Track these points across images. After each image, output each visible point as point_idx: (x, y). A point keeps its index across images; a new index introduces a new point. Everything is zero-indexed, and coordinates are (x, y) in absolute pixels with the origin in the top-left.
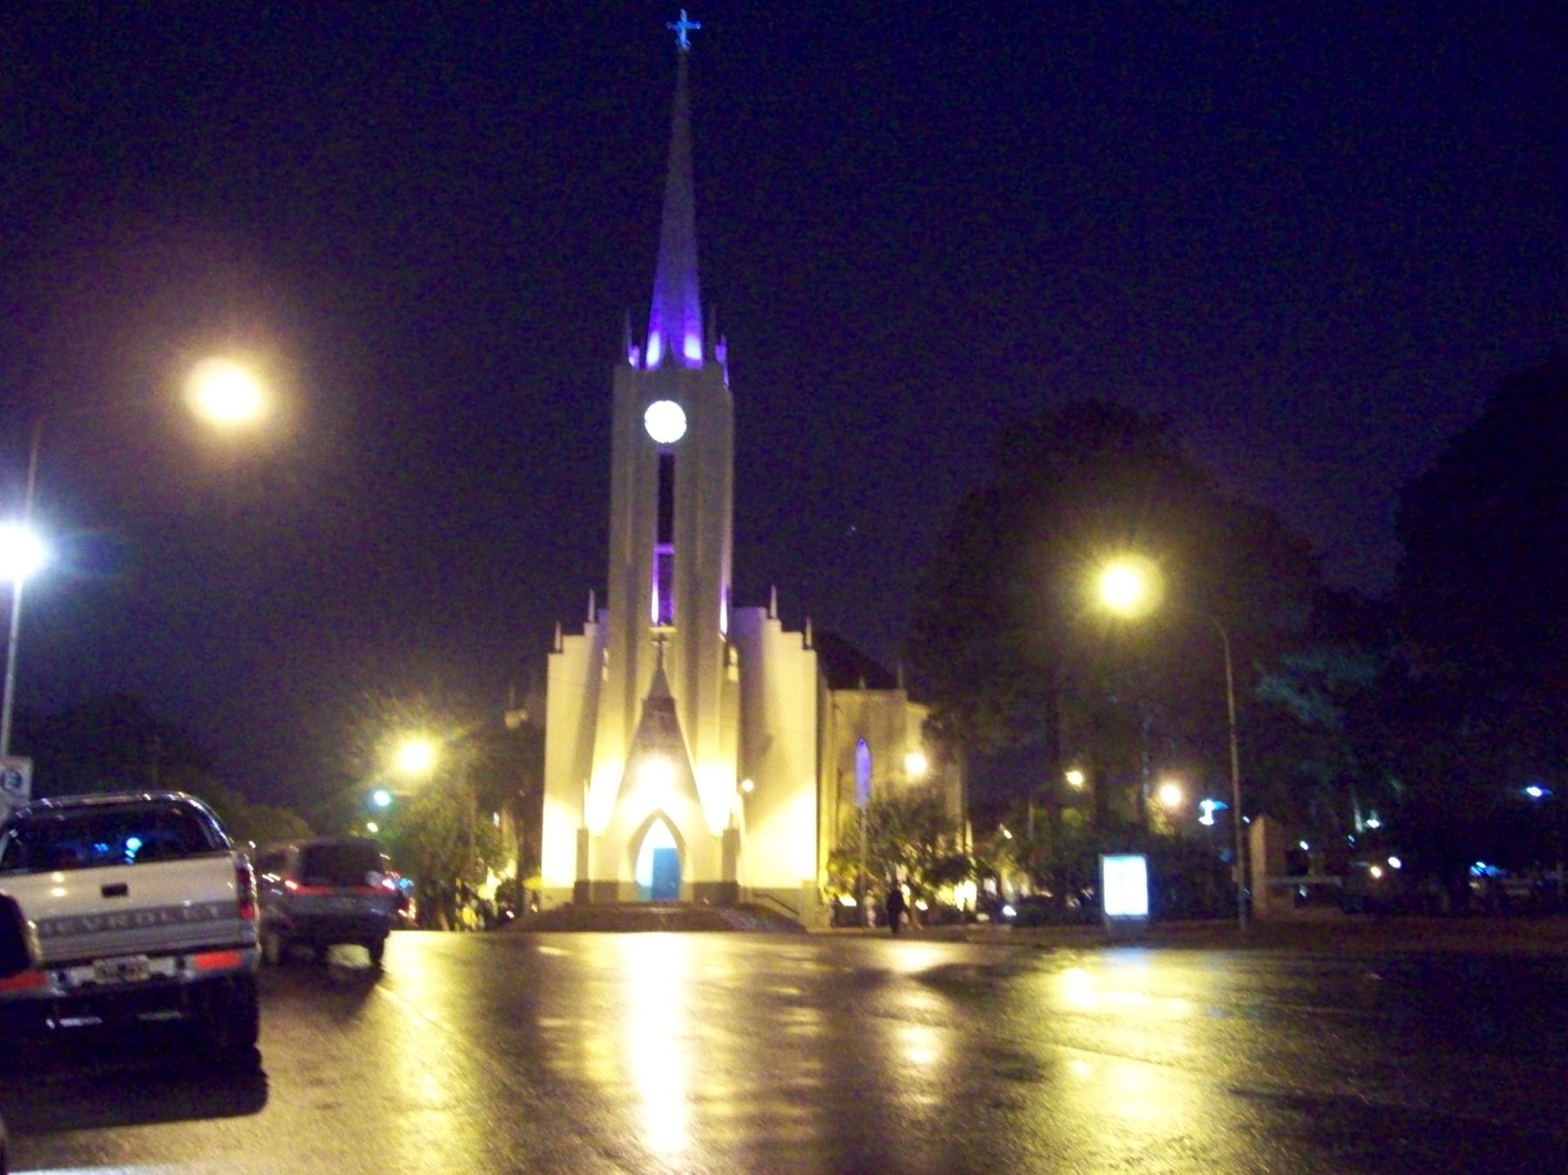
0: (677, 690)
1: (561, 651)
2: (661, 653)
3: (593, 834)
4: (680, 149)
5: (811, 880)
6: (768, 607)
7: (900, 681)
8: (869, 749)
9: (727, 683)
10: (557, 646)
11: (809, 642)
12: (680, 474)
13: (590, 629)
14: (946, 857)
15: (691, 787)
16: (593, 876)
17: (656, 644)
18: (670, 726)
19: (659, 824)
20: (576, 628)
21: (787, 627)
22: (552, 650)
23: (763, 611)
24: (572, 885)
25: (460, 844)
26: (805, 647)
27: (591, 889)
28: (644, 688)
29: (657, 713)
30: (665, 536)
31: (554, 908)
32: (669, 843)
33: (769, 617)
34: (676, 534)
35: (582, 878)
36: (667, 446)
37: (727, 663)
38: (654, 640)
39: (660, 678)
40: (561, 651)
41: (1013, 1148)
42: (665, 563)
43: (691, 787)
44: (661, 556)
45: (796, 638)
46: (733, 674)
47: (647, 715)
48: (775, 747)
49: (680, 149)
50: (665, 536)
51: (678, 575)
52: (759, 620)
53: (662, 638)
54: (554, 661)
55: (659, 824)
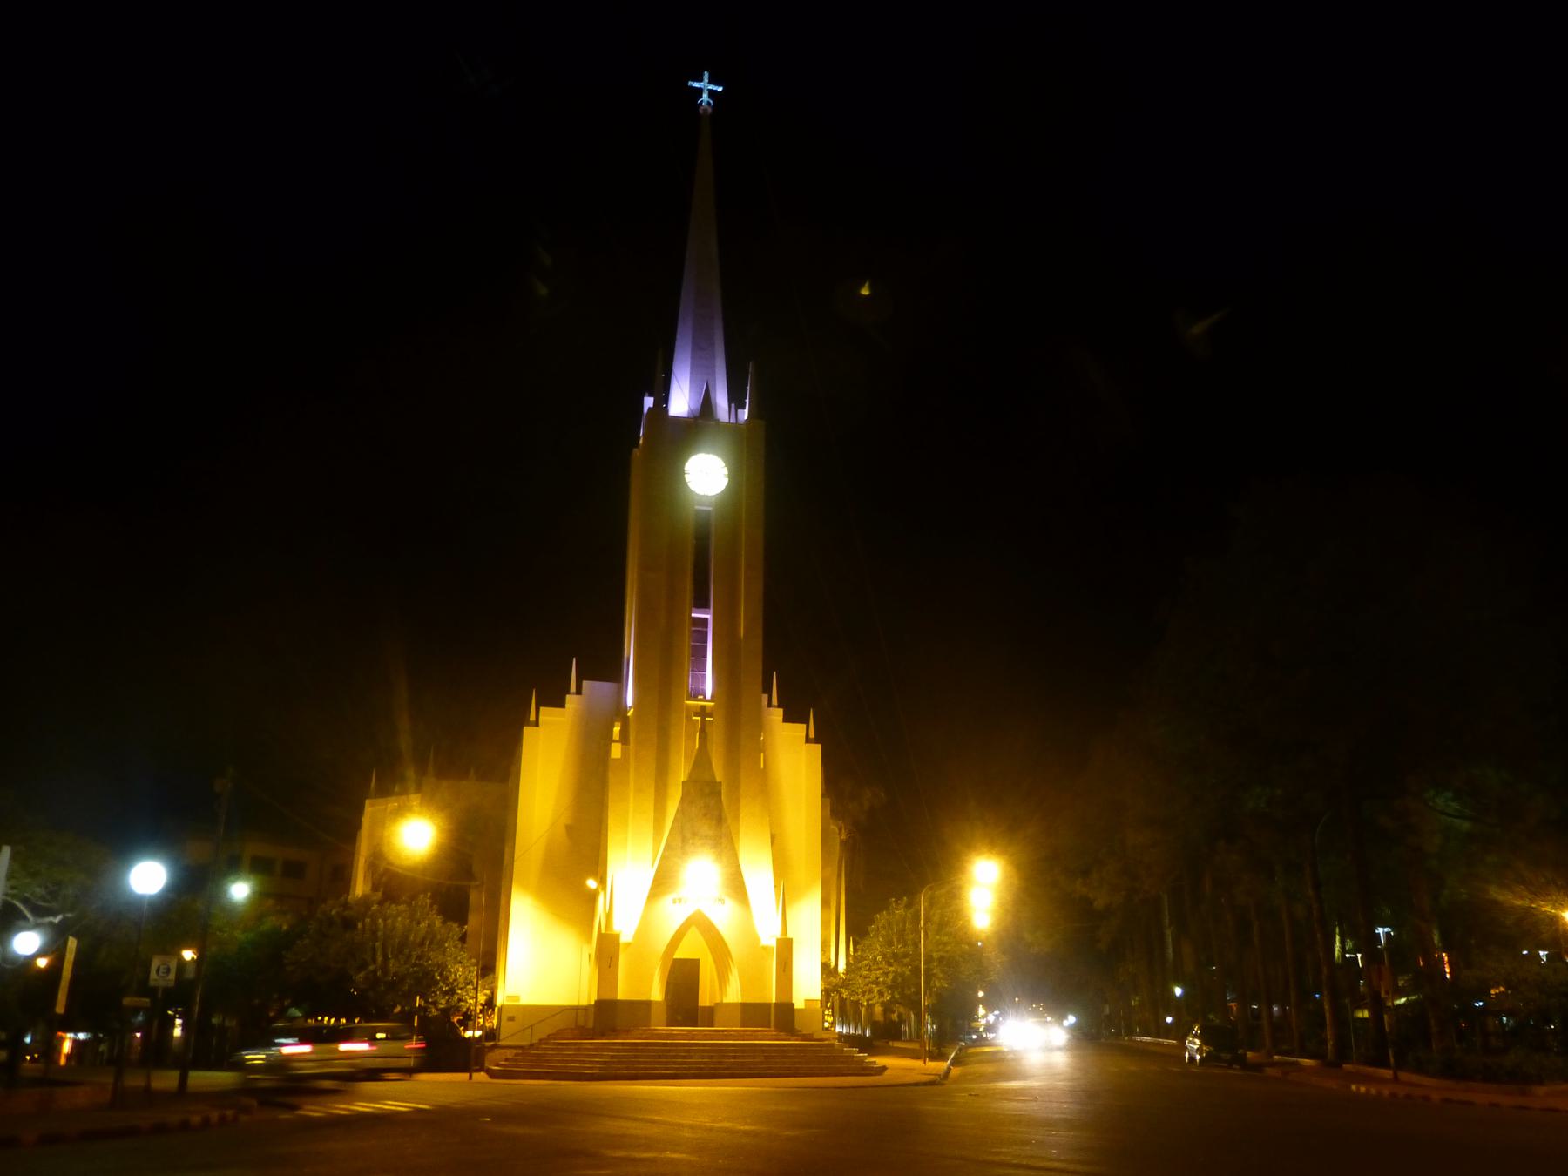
1: (537, 724)
10: (532, 717)
11: (812, 735)
13: (572, 701)
15: (737, 886)
19: (693, 935)
26: (808, 740)
35: (607, 996)
40: (537, 724)
43: (737, 886)
45: (798, 730)
55: (693, 935)
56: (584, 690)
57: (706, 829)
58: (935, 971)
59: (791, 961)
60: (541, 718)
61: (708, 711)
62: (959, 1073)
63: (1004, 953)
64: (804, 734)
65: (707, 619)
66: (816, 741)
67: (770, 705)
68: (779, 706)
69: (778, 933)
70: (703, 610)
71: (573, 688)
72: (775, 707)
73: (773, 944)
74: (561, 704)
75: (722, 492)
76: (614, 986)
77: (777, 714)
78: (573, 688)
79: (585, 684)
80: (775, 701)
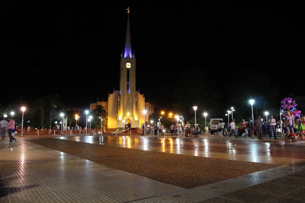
13: (114, 93)
26: (143, 97)
30: (128, 81)
33: (138, 92)
42: (128, 84)
50: (128, 81)
64: (142, 96)
67: (138, 92)
74: (112, 93)
77: (139, 93)
79: (116, 91)
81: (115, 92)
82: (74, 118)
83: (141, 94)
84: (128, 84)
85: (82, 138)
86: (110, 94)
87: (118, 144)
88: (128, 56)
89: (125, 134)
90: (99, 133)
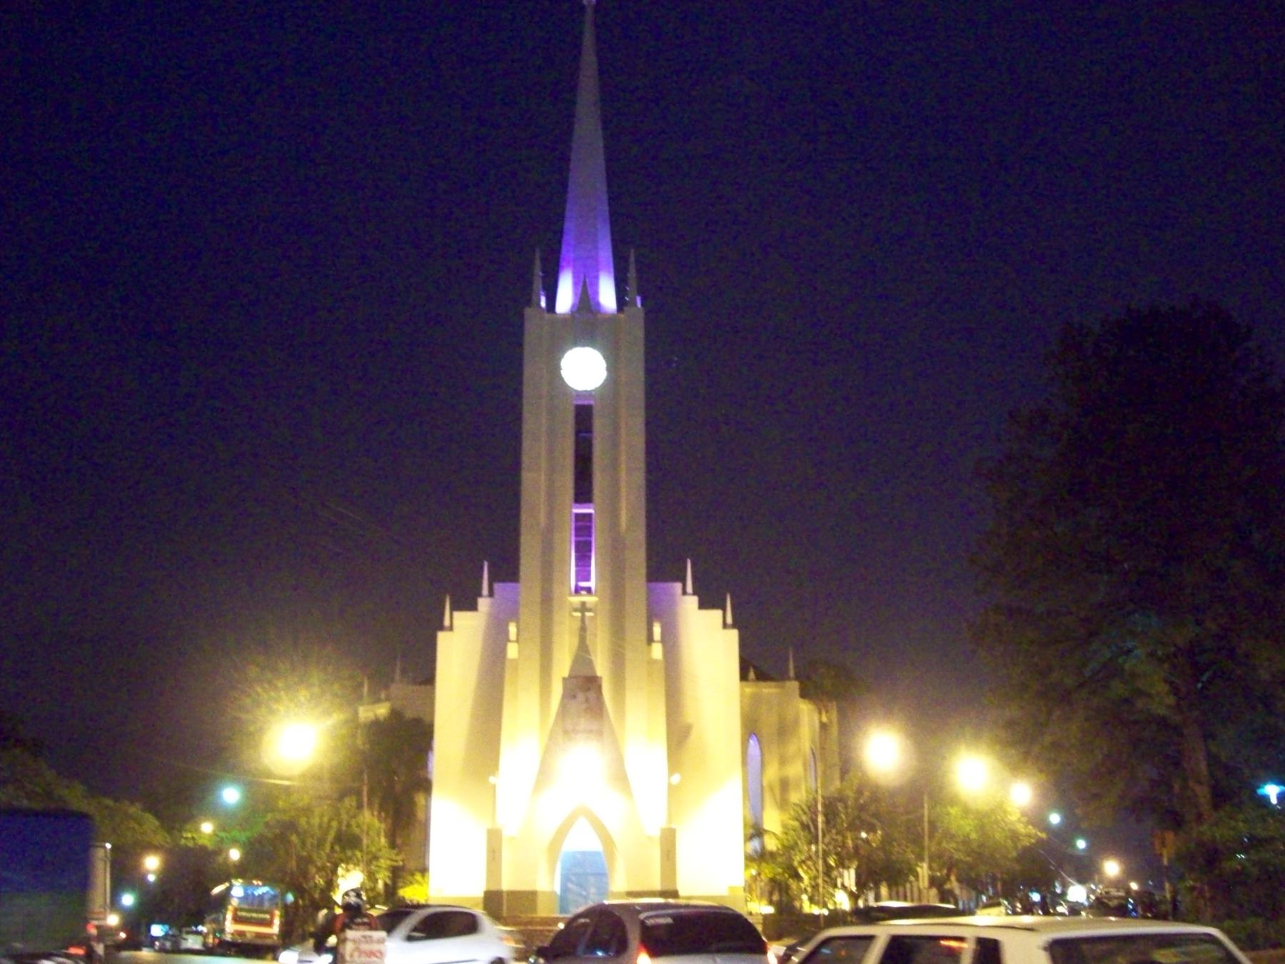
0: (602, 668)
1: (451, 628)
2: (583, 629)
3: (506, 835)
4: (589, 60)
5: (362, 880)
6: (683, 580)
7: (792, 673)
8: (760, 742)
9: (652, 662)
10: (447, 622)
11: (729, 620)
12: (600, 427)
13: (484, 603)
14: (1105, 843)
15: (621, 777)
16: (506, 885)
17: (578, 614)
18: (596, 709)
19: (582, 825)
20: (467, 603)
21: (706, 603)
22: (441, 627)
23: (678, 586)
24: (481, 895)
25: (337, 848)
26: (725, 626)
27: (505, 895)
28: (563, 666)
29: (581, 697)
30: (583, 493)
31: (972, 960)
32: (594, 845)
33: (684, 593)
34: (597, 492)
35: (494, 888)
36: (587, 394)
37: (650, 640)
38: (576, 610)
39: (583, 655)
40: (451, 628)
41: (73, 951)
42: (583, 526)
43: (621, 777)
44: (579, 517)
45: (716, 615)
46: (657, 651)
47: (569, 695)
48: (694, 736)
49: (589, 60)
50: (583, 493)
51: (597, 540)
52: (673, 595)
53: (583, 608)
54: (442, 637)
55: (582, 825)
56: (496, 591)
57: (583, 723)
58: (1217, 835)
59: (675, 854)
60: (456, 622)
61: (588, 606)
62: (1162, 952)
63: (981, 828)
64: (720, 620)
65: (590, 515)
66: (734, 626)
67: (684, 593)
68: (694, 593)
69: (662, 823)
70: (586, 505)
71: (485, 591)
72: (690, 594)
73: (657, 834)
74: (473, 607)
75: (600, 386)
76: (499, 881)
77: (692, 602)
78: (485, 591)
79: (496, 586)
80: (689, 588)
81: (491, 594)
82: (1150, 885)
83: (703, 605)
84: (583, 526)
85: (118, 930)
86: (457, 614)
87: (712, 943)
88: (586, 299)
89: (859, 854)
90: (839, 849)
